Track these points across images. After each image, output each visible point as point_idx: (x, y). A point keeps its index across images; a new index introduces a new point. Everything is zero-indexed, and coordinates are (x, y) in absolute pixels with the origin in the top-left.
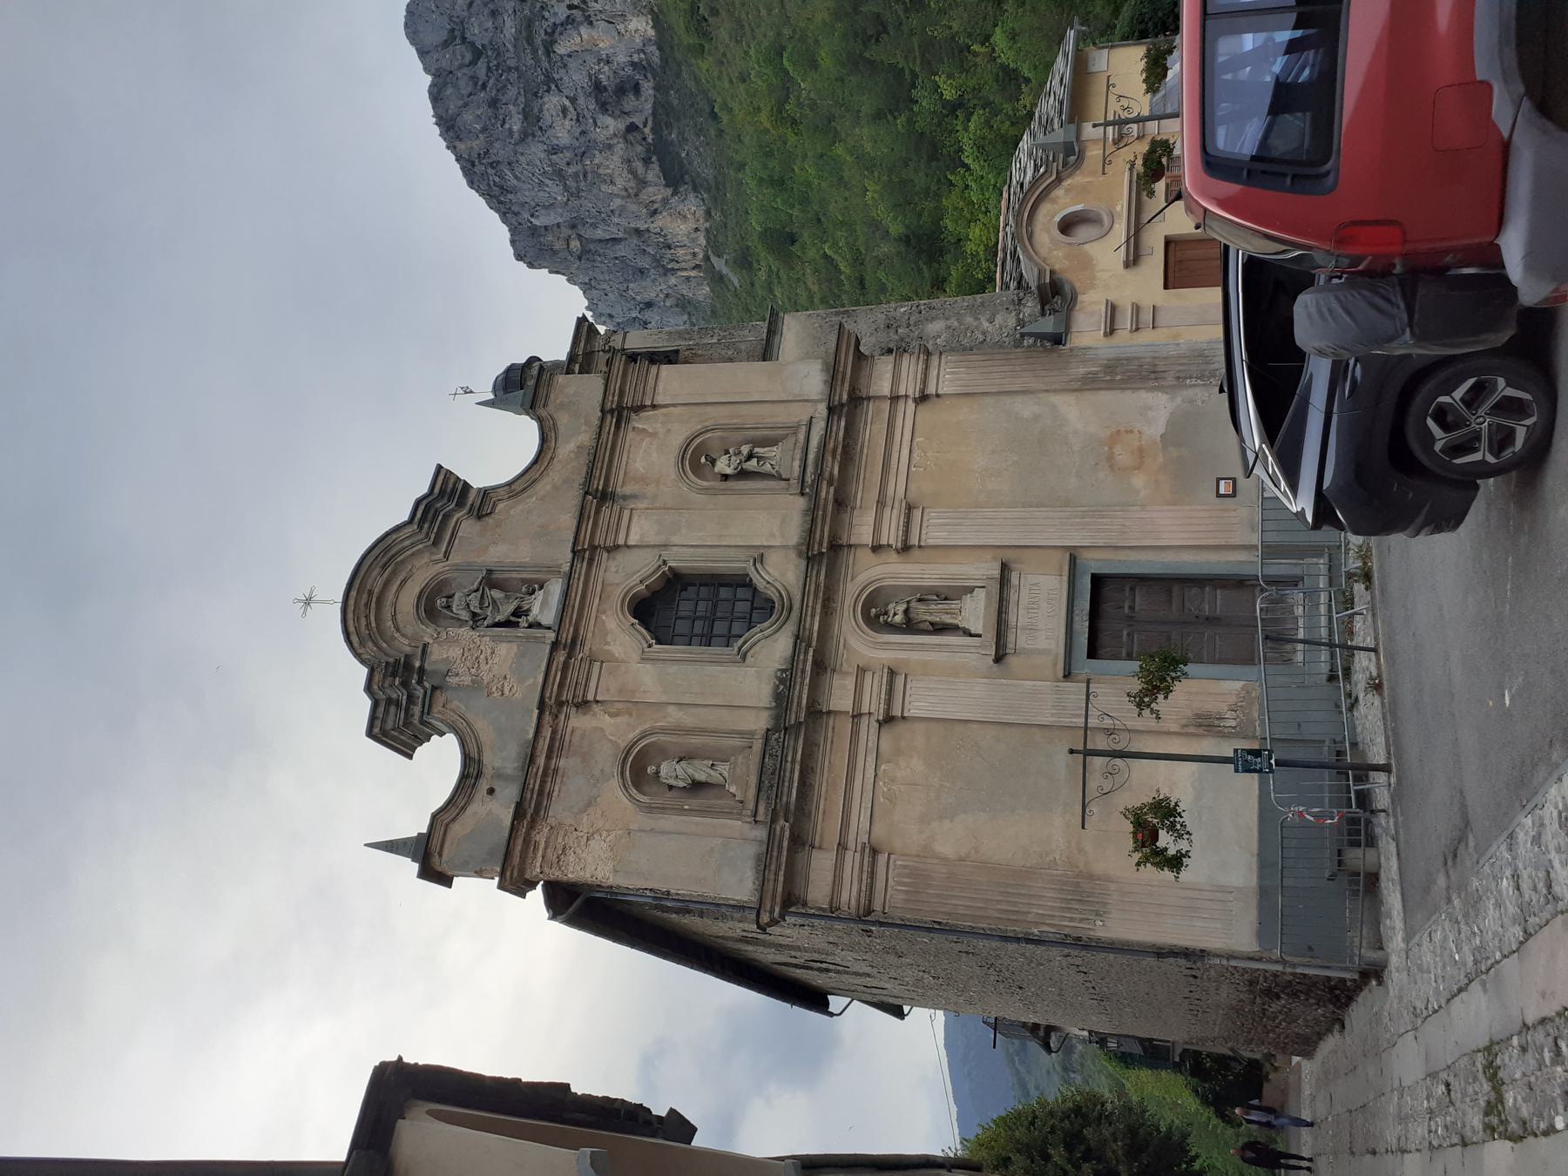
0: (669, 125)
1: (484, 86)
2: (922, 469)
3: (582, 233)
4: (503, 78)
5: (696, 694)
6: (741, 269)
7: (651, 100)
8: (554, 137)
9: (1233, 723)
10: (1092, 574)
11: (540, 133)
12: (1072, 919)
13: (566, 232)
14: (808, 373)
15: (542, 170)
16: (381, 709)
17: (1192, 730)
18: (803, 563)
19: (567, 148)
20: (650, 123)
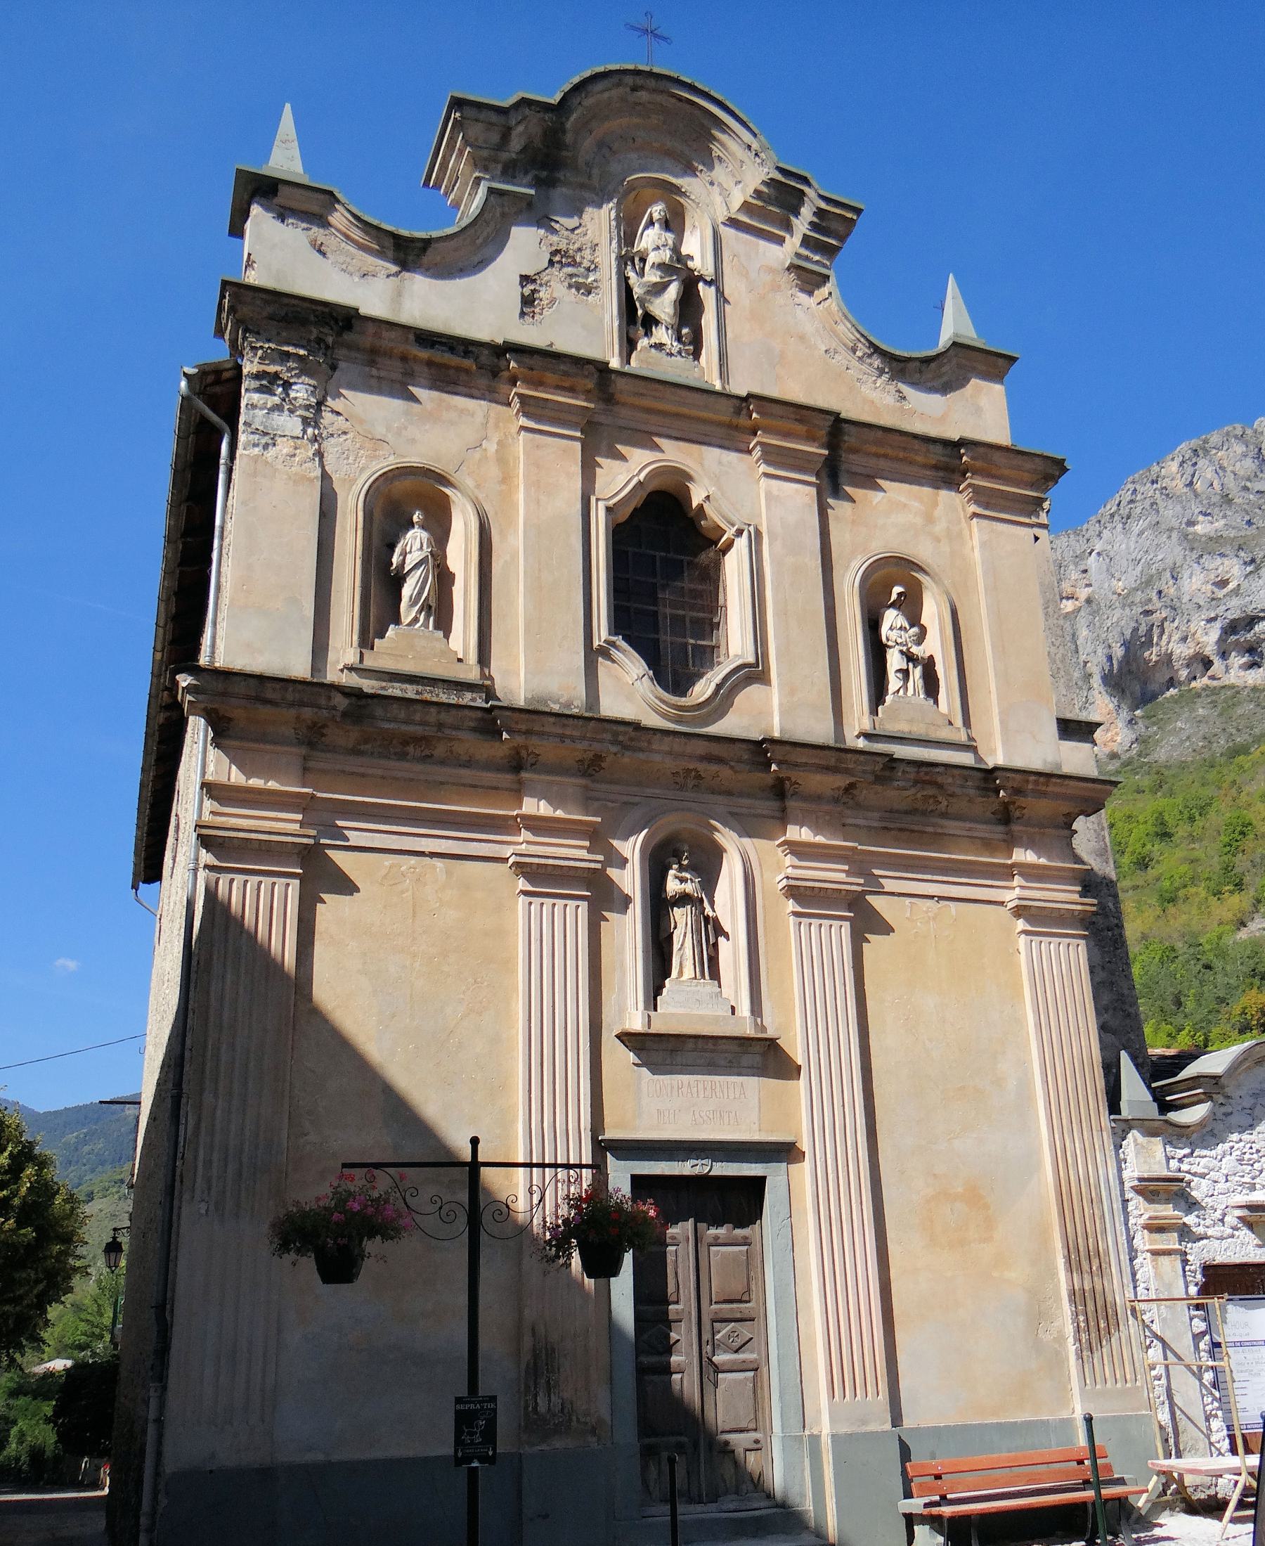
0: (1214, 704)
1: (1246, 489)
3: (1082, 613)
4: (1257, 510)
7: (1239, 683)
8: (1192, 573)
9: (542, 1408)
10: (764, 1178)
11: (1194, 556)
12: (208, 1163)
13: (1083, 594)
15: (1151, 562)
16: (494, 117)
17: (527, 1342)
19: (1178, 589)
20: (1215, 683)
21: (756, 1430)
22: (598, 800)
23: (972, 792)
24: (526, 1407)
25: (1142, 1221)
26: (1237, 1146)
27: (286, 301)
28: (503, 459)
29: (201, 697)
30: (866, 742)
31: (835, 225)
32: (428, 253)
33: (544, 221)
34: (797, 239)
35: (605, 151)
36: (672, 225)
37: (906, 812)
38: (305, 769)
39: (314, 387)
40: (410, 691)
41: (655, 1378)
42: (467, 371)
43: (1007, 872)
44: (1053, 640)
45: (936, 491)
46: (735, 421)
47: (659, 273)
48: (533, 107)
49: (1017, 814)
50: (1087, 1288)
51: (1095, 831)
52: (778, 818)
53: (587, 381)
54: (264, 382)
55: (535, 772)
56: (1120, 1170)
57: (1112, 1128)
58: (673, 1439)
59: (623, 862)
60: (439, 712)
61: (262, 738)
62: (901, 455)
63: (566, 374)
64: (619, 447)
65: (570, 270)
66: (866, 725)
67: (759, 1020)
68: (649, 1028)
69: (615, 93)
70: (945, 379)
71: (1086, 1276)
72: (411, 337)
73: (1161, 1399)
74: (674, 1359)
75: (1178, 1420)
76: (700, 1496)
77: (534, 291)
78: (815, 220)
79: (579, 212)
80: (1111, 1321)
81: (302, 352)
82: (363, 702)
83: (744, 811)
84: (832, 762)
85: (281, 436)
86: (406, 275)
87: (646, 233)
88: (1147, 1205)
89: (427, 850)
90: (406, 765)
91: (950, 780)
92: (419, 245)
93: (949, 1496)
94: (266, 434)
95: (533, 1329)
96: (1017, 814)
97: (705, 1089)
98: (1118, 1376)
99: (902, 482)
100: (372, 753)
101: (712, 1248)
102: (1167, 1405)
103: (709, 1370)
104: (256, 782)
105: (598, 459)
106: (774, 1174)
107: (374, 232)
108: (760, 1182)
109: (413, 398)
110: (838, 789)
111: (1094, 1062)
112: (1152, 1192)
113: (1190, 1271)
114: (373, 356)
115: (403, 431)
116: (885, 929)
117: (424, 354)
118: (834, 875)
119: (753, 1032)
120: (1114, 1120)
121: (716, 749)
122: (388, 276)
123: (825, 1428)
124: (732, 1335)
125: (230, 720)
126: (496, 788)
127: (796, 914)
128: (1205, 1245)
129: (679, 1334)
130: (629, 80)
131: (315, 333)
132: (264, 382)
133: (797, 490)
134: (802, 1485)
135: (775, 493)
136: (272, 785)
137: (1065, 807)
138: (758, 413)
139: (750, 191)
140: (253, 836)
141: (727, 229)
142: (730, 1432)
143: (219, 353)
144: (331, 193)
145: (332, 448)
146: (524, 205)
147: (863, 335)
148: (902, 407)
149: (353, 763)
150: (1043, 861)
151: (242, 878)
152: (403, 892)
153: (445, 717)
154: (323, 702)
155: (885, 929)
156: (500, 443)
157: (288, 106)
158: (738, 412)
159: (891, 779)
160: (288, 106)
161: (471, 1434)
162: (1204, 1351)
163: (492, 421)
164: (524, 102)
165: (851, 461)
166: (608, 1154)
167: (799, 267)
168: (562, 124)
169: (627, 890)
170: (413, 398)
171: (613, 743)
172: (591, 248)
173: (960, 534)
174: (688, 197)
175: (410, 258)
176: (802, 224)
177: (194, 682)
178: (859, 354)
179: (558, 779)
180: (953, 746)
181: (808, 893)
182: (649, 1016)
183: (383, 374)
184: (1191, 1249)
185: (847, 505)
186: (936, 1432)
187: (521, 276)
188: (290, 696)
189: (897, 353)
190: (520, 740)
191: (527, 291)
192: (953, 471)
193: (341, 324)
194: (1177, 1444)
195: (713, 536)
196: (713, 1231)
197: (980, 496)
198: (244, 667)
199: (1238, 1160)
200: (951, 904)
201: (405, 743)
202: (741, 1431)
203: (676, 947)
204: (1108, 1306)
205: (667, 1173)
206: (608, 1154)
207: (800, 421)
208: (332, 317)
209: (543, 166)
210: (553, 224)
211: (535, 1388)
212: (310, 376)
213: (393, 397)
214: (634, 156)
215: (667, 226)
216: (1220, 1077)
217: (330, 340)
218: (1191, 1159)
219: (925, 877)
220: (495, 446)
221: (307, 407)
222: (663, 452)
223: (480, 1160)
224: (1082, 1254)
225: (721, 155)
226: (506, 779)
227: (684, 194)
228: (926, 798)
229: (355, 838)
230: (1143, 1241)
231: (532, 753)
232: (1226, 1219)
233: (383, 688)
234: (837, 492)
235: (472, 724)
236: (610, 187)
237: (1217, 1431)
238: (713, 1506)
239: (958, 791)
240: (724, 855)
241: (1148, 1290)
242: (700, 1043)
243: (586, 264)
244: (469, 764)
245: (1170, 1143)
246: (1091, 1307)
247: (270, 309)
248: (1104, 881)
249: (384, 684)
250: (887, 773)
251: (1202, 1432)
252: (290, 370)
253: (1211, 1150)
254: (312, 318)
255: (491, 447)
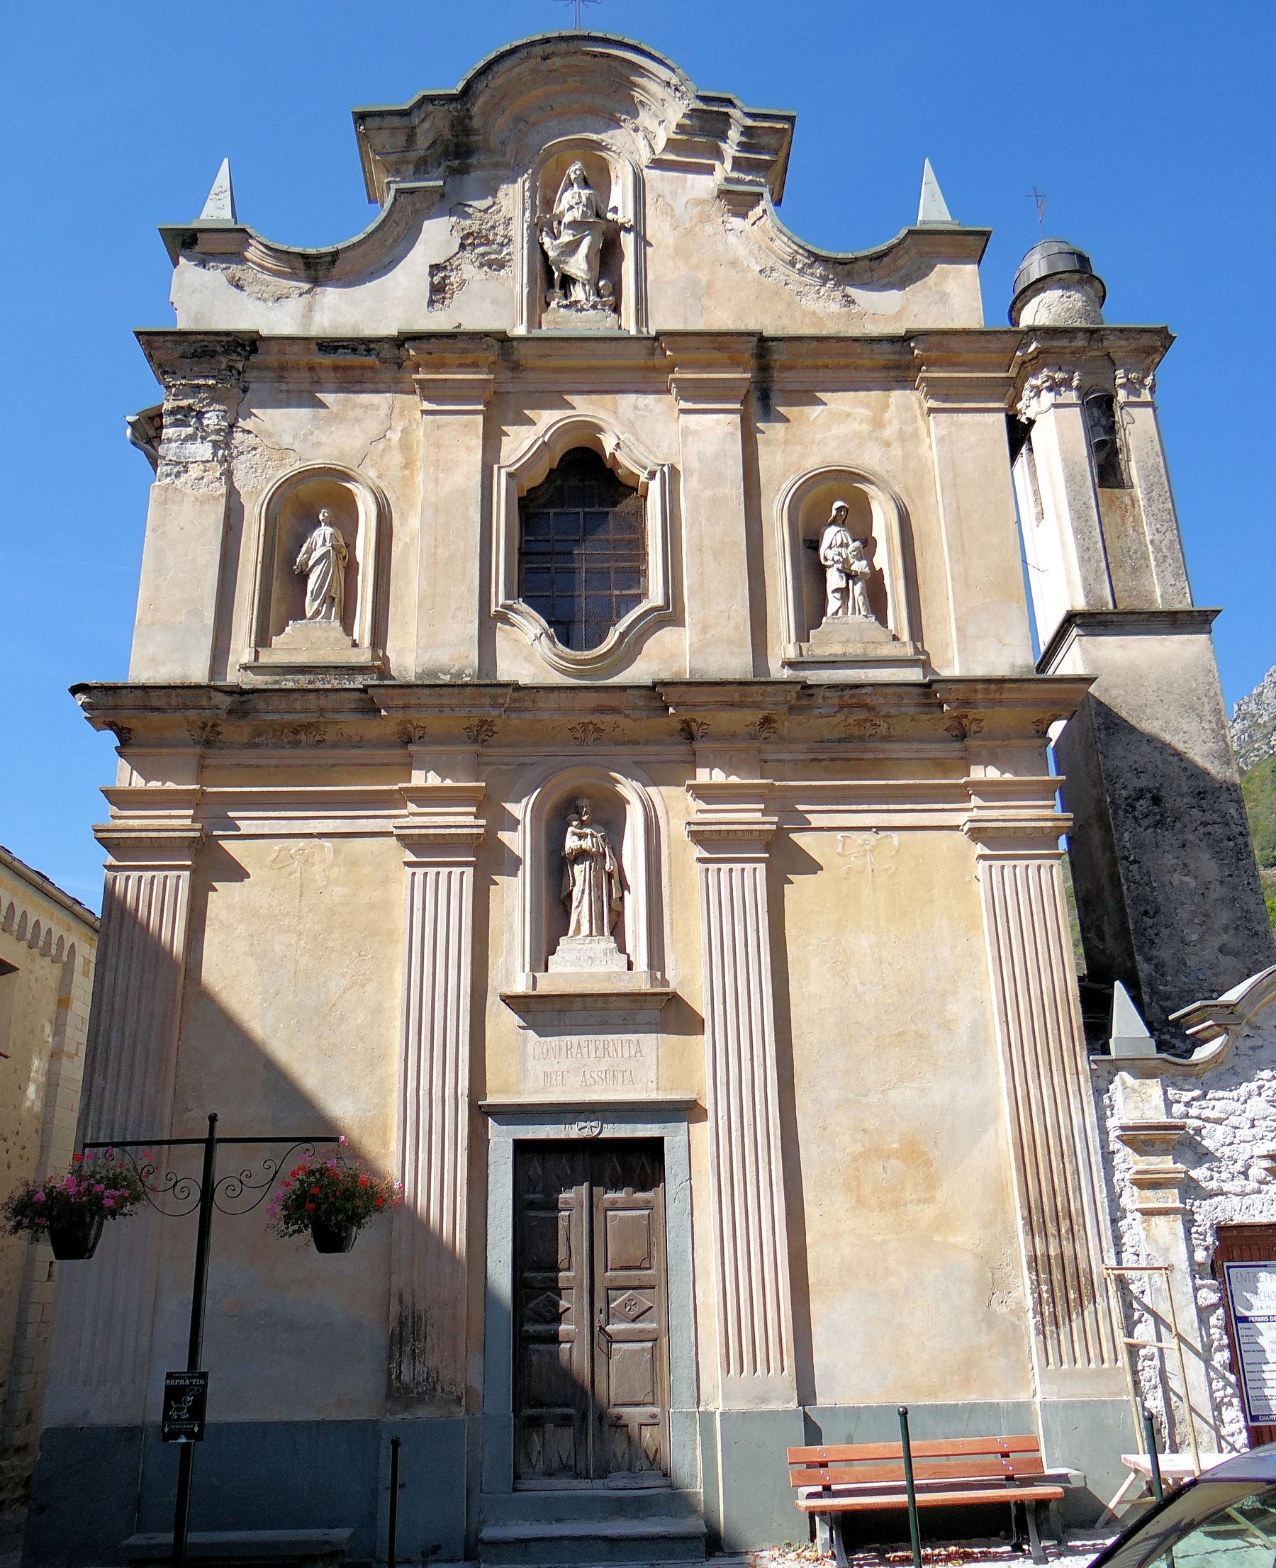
2: (840, 850)
5: (435, 554)
6: (160, 442)
9: (406, 1377)
10: (662, 1139)
14: (1005, 645)
16: (396, 121)
17: (394, 1309)
18: (649, 682)
21: (653, 1404)
22: (492, 764)
23: (911, 710)
24: (390, 1374)
25: (1128, 1176)
26: (1267, 1085)
27: (193, 338)
28: (405, 445)
29: (96, 713)
30: (791, 672)
31: (764, 140)
32: (337, 264)
33: (457, 208)
34: (728, 164)
35: (522, 125)
36: (590, 181)
37: (840, 741)
38: (202, 767)
39: (225, 411)
40: (303, 681)
41: (542, 1347)
42: (372, 368)
43: (961, 794)
44: (1158, 526)
45: (887, 393)
46: (650, 363)
47: (571, 232)
48: (436, 102)
49: (974, 727)
50: (1052, 1253)
51: (1213, 730)
52: (689, 762)
53: (486, 354)
54: (179, 416)
55: (425, 744)
56: (1101, 1119)
57: (1091, 1069)
58: (559, 1411)
59: (513, 824)
60: (319, 698)
61: (162, 743)
62: (843, 362)
63: (464, 351)
64: (526, 412)
65: (481, 250)
66: (791, 653)
67: (659, 975)
68: (534, 989)
69: (525, 67)
70: (903, 272)
71: (1051, 1240)
72: (314, 347)
73: (1153, 1382)
74: (563, 1327)
75: (1173, 1408)
76: (587, 1470)
77: (444, 278)
78: (744, 139)
79: (493, 192)
80: (1084, 1291)
81: (211, 382)
82: (245, 698)
83: (652, 758)
84: (736, 698)
85: (192, 463)
86: (318, 290)
87: (565, 194)
88: (1137, 1157)
89: (314, 831)
90: (298, 752)
91: (881, 700)
92: (329, 259)
93: (833, 1487)
94: (178, 463)
95: (401, 1296)
96: (974, 727)
97: (597, 1048)
98: (1092, 1355)
99: (845, 391)
100: (267, 744)
101: (610, 1213)
102: (1160, 1390)
103: (600, 1339)
104: (155, 785)
105: (504, 428)
106: (673, 1136)
107: (285, 256)
108: (659, 1142)
109: (322, 405)
110: (753, 724)
111: (1070, 997)
112: (1144, 1142)
113: (1197, 1232)
114: (282, 370)
115: (310, 437)
116: (811, 867)
117: (328, 360)
118: (749, 816)
119: (648, 987)
120: (1095, 1062)
121: (606, 700)
122: (301, 295)
123: (715, 1403)
124: (628, 1303)
125: (129, 730)
126: (388, 765)
127: (700, 860)
128: (1220, 1203)
129: (570, 1302)
130: (538, 50)
131: (224, 361)
132: (179, 416)
133: (718, 421)
134: (693, 1465)
135: (693, 427)
136: (170, 785)
137: (1033, 714)
138: (670, 350)
139: (673, 127)
140: (144, 834)
141: (652, 171)
142: (624, 1405)
143: (1044, 391)
144: (244, 230)
145: (240, 467)
146: (436, 197)
147: (800, 247)
148: (850, 311)
149: (250, 757)
150: (1008, 776)
151: (434, 870)
152: (291, 874)
153: (324, 702)
154: (204, 702)
155: (811, 867)
156: (404, 431)
157: (226, 161)
158: (652, 353)
159: (810, 707)
160: (226, 161)
161: (178, 1409)
162: (1216, 1327)
163: (396, 411)
164: (427, 99)
165: (783, 380)
166: (490, 1119)
167: (728, 192)
168: (468, 110)
169: (519, 853)
170: (322, 405)
171: (493, 706)
172: (504, 223)
173: (915, 434)
174: (609, 150)
175: (321, 273)
176: (730, 149)
177: (87, 700)
178: (799, 266)
179: (446, 748)
180: (887, 663)
181: (715, 837)
182: (535, 978)
183: (291, 387)
184: (1200, 1206)
185: (779, 427)
186: (855, 1413)
187: (431, 266)
188: (174, 702)
189: (840, 256)
190: (399, 715)
191: (436, 280)
192: (908, 367)
193: (248, 349)
194: (1172, 1435)
195: (631, 484)
196: (611, 1195)
197: (936, 390)
198: (148, 679)
199: (1269, 1102)
200: (893, 834)
201: (296, 732)
202: (637, 1405)
203: (575, 904)
204: (1081, 1274)
205: (552, 1136)
206: (490, 1119)
207: (719, 349)
208: (239, 345)
209: (457, 155)
210: (466, 209)
211: (400, 1356)
212: (221, 403)
213: (301, 406)
214: (553, 123)
215: (586, 183)
216: (1235, 1005)
217: (240, 366)
218: (1203, 1103)
219: (860, 807)
220: (399, 434)
221: (218, 432)
222: (574, 408)
223: (217, 1136)
224: (1047, 1214)
225: (643, 99)
226: (678, 751)
227: (605, 148)
228: (860, 723)
229: (246, 827)
230: (1131, 1199)
231: (418, 726)
232: (1250, 1172)
233: (276, 682)
234: (768, 413)
235: (353, 706)
236: (526, 161)
237: (1231, 1422)
238: (599, 1483)
239: (893, 711)
240: (627, 806)
241: (1138, 1255)
242: (589, 1001)
243: (499, 239)
244: (360, 744)
245: (1174, 1085)
246: (1057, 1275)
247: (180, 349)
248: (1224, 785)
249: (277, 678)
250: (805, 702)
251: (1207, 1423)
252: (201, 401)
253: (1231, 1091)
254: (219, 349)
255: (395, 436)
